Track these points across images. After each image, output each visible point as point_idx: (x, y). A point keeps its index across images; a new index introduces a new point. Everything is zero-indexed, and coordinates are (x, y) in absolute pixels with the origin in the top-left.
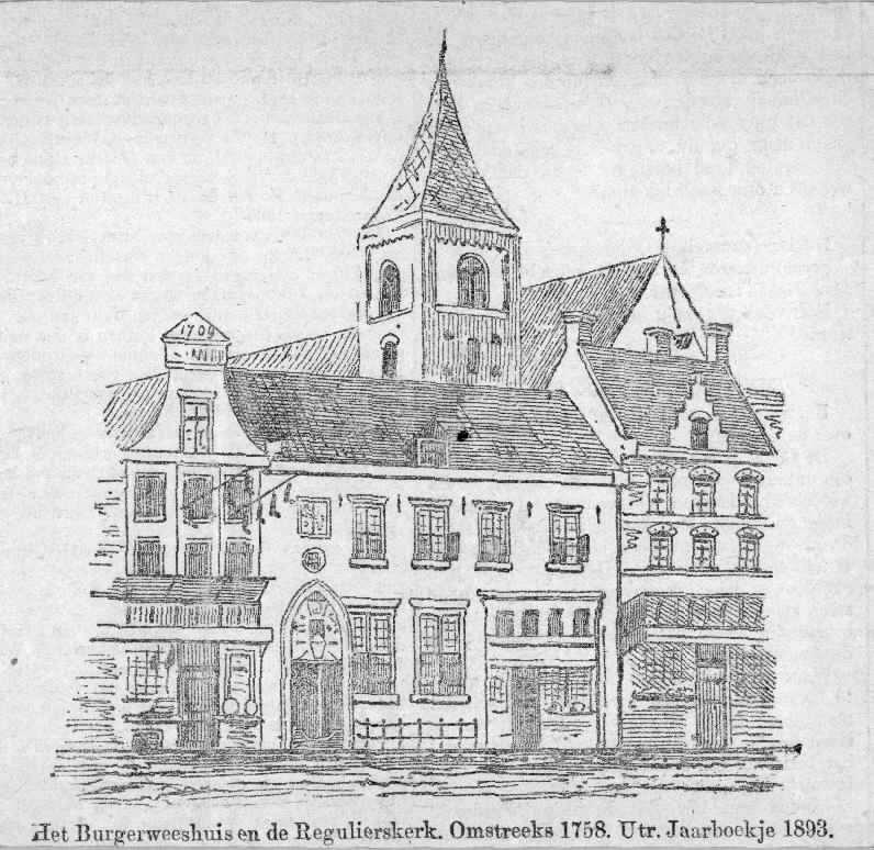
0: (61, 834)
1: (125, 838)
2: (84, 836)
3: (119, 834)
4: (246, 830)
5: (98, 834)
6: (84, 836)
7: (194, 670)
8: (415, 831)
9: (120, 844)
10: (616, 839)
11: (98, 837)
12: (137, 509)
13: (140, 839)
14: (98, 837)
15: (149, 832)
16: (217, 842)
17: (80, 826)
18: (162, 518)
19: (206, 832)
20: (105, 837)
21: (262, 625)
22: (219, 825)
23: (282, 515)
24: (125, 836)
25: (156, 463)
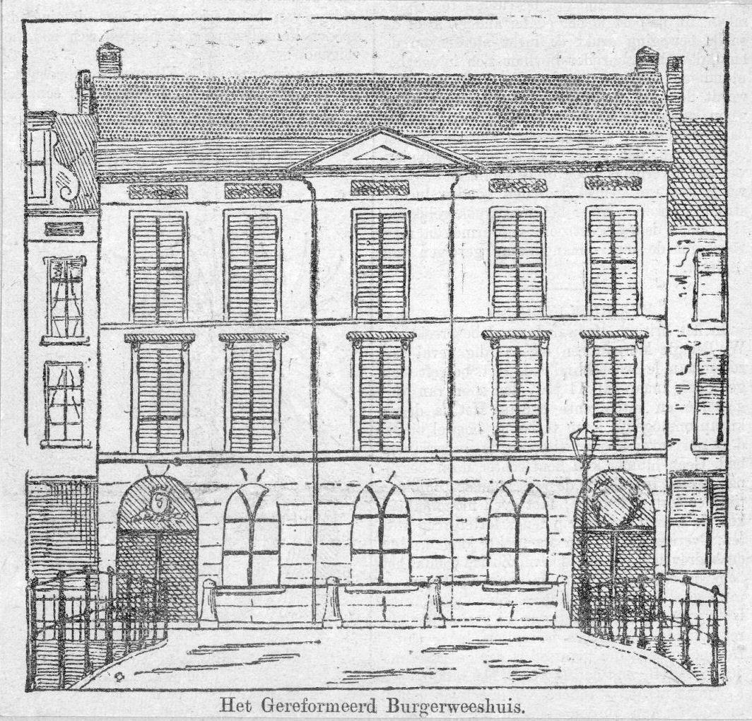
0: (245, 706)
1: (429, 710)
2: (394, 708)
3: (424, 707)
4: (357, 703)
5: (405, 706)
6: (394, 708)
7: (123, 630)
8: (439, 706)
9: (424, 715)
10: (257, 711)
11: (501, 710)
12: (79, 408)
13: (287, 711)
14: (501, 710)
15: (449, 705)
16: (335, 713)
17: (390, 699)
18: (355, 212)
19: (499, 705)
20: (411, 709)
21: (449, 517)
22: (510, 699)
23: (481, 337)
24: (429, 708)
25: (147, 205)
